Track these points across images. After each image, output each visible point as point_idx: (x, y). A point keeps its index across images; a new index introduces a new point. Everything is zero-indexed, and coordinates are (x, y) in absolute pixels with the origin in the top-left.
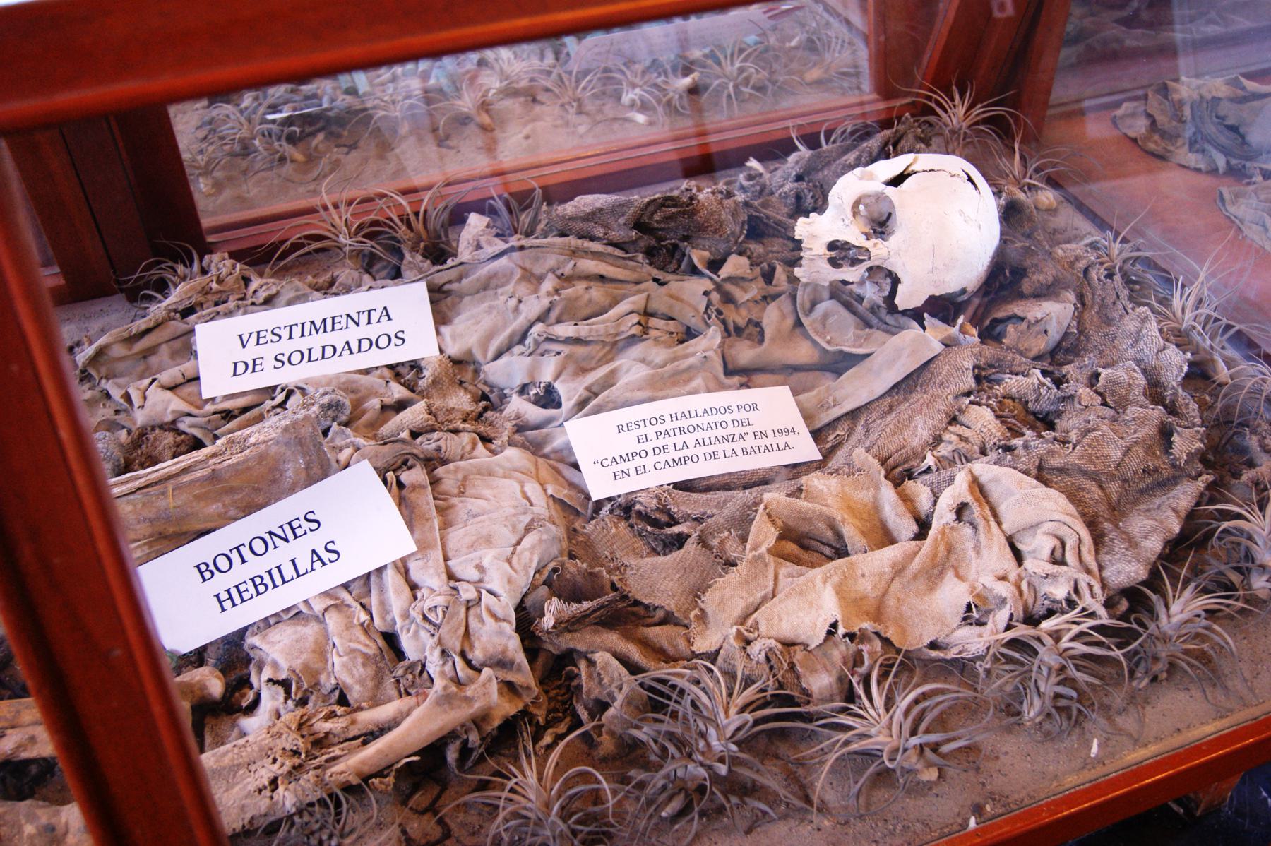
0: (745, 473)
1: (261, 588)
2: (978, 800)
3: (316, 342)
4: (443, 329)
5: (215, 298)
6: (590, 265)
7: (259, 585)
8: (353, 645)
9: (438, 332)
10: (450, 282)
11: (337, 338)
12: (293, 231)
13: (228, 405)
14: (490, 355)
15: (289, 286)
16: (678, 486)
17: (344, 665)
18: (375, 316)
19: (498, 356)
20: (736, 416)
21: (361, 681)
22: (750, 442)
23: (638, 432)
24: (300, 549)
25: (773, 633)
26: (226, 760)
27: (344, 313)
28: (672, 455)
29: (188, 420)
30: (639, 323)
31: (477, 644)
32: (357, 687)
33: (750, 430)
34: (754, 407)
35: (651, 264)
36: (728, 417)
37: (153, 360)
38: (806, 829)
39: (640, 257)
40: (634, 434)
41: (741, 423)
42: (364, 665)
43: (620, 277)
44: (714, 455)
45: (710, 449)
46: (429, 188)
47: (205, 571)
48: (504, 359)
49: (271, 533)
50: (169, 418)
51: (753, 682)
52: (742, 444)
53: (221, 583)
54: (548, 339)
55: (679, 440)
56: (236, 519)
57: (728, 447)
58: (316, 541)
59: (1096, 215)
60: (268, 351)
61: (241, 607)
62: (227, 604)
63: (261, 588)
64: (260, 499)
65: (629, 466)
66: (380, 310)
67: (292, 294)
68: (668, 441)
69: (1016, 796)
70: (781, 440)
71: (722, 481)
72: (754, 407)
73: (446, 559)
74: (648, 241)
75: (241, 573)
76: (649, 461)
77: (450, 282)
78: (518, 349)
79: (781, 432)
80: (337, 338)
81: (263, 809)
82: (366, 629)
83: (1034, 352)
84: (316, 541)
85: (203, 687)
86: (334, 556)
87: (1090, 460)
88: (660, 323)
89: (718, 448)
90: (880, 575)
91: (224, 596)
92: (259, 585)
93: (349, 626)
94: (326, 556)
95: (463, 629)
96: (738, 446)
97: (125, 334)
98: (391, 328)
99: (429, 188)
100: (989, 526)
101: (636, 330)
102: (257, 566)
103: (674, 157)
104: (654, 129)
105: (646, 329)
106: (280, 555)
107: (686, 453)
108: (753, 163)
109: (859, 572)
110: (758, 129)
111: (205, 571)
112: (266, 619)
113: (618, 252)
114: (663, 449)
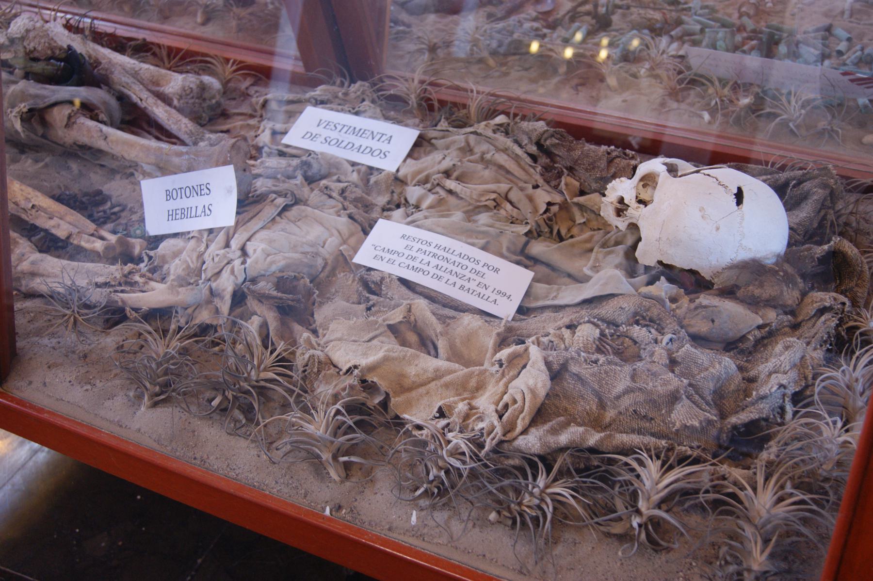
0: (453, 300)
2: (343, 504)
5: (340, 102)
6: (502, 159)
8: (188, 259)
9: (405, 161)
10: (436, 138)
11: (358, 141)
13: (285, 150)
16: (404, 282)
17: (177, 265)
20: (479, 268)
22: (473, 285)
23: (409, 243)
25: (330, 354)
27: (371, 130)
28: (416, 264)
30: (494, 200)
31: (218, 281)
33: (479, 279)
34: (497, 270)
35: (542, 175)
36: (471, 265)
38: (254, 452)
40: (406, 242)
41: (477, 273)
42: (183, 269)
43: (516, 173)
44: (439, 278)
45: (440, 273)
52: (466, 283)
55: (427, 259)
57: (453, 279)
59: (176, 35)
65: (388, 256)
66: (389, 136)
68: (421, 256)
69: (364, 518)
70: (493, 297)
71: (433, 294)
72: (497, 270)
73: (249, 240)
74: (544, 160)
76: (400, 260)
77: (436, 138)
79: (499, 292)
80: (358, 141)
83: (692, 330)
85: (133, 247)
87: (599, 382)
88: (509, 207)
89: (447, 276)
90: (425, 371)
93: (194, 250)
95: (218, 270)
96: (459, 283)
97: (280, 98)
100: (501, 380)
101: (491, 204)
103: (710, 148)
105: (497, 206)
107: (425, 268)
109: (416, 362)
111: (169, 195)
114: (414, 259)
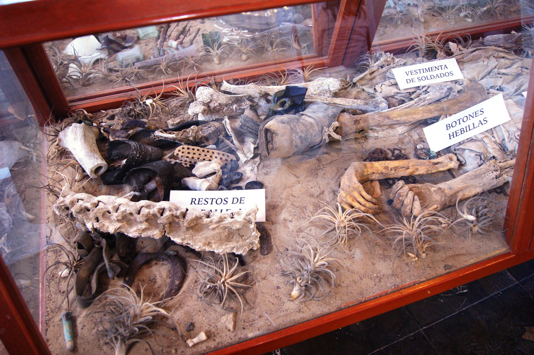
1: (463, 132)
3: (428, 74)
4: (463, 71)
7: (462, 131)
12: (410, 44)
14: (480, 78)
15: (410, 60)
18: (443, 67)
19: (482, 79)
21: (499, 155)
24: (476, 120)
26: (478, 173)
29: (399, 95)
32: (499, 157)
37: (374, 81)
39: (513, 52)
46: (437, 34)
47: (448, 127)
48: (485, 80)
49: (470, 115)
50: (392, 94)
51: (417, 217)
53: (452, 130)
54: (499, 73)
56: (462, 110)
58: (481, 118)
60: (415, 77)
61: (456, 138)
62: (452, 137)
63: (463, 132)
64: (468, 105)
67: (411, 62)
75: (458, 127)
78: (488, 76)
80: (434, 73)
81: (495, 183)
82: (495, 142)
84: (481, 118)
86: (485, 122)
91: (451, 134)
92: (462, 131)
94: (483, 122)
98: (448, 71)
99: (437, 34)
102: (463, 125)
104: (473, 24)
106: (470, 122)
108: (513, 32)
110: (476, 29)
111: (448, 127)
112: (459, 143)
113: (507, 51)
